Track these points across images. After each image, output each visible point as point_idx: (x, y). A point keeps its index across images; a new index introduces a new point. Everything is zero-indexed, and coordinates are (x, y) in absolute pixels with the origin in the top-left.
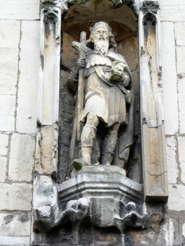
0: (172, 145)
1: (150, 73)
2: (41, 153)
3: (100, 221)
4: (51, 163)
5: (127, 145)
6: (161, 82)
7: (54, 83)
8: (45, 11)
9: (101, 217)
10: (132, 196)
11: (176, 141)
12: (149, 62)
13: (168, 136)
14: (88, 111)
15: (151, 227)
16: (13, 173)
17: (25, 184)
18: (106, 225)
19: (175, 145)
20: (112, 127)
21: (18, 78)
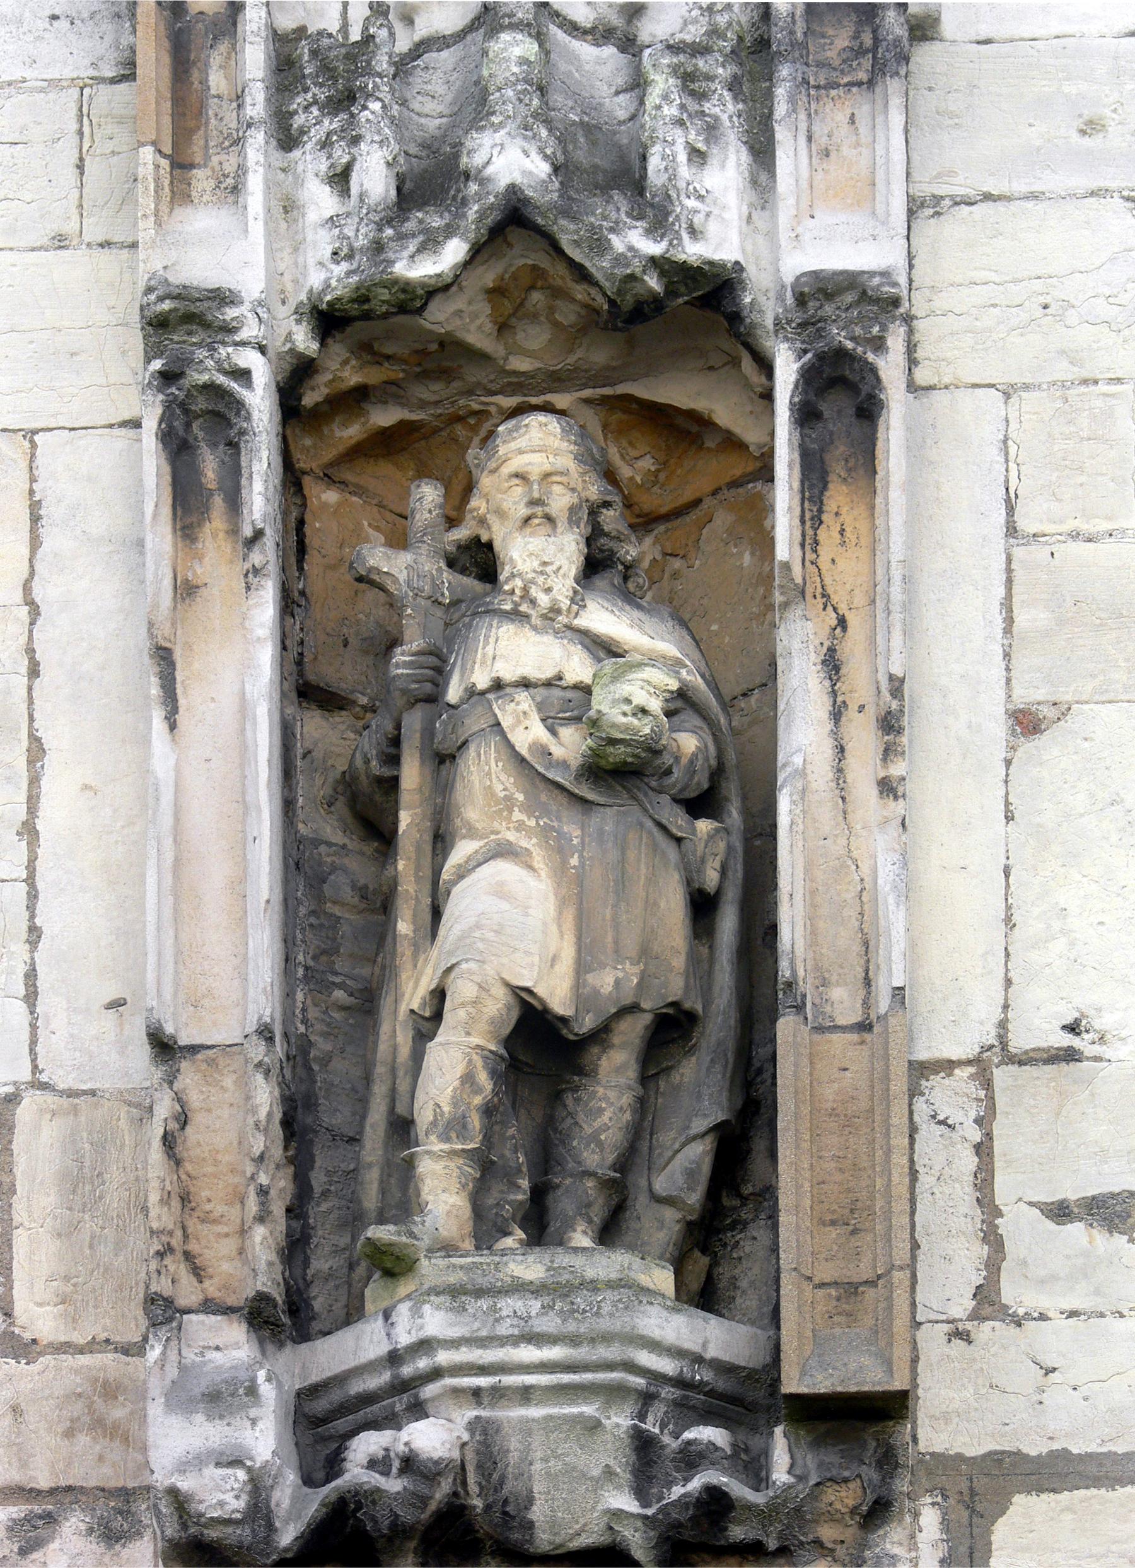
0: (961, 1112)
1: (837, 714)
2: (185, 1198)
3: (531, 1525)
4: (241, 1251)
5: (700, 1125)
6: (897, 769)
7: (245, 806)
8: (168, 377)
9: (535, 1508)
10: (712, 1393)
11: (982, 1094)
12: (832, 650)
13: (922, 1070)
14: (451, 953)
15: (818, 1543)
16: (40, 1305)
17: (110, 1356)
18: (561, 1546)
19: (973, 1114)
20: (600, 1035)
21: (34, 781)
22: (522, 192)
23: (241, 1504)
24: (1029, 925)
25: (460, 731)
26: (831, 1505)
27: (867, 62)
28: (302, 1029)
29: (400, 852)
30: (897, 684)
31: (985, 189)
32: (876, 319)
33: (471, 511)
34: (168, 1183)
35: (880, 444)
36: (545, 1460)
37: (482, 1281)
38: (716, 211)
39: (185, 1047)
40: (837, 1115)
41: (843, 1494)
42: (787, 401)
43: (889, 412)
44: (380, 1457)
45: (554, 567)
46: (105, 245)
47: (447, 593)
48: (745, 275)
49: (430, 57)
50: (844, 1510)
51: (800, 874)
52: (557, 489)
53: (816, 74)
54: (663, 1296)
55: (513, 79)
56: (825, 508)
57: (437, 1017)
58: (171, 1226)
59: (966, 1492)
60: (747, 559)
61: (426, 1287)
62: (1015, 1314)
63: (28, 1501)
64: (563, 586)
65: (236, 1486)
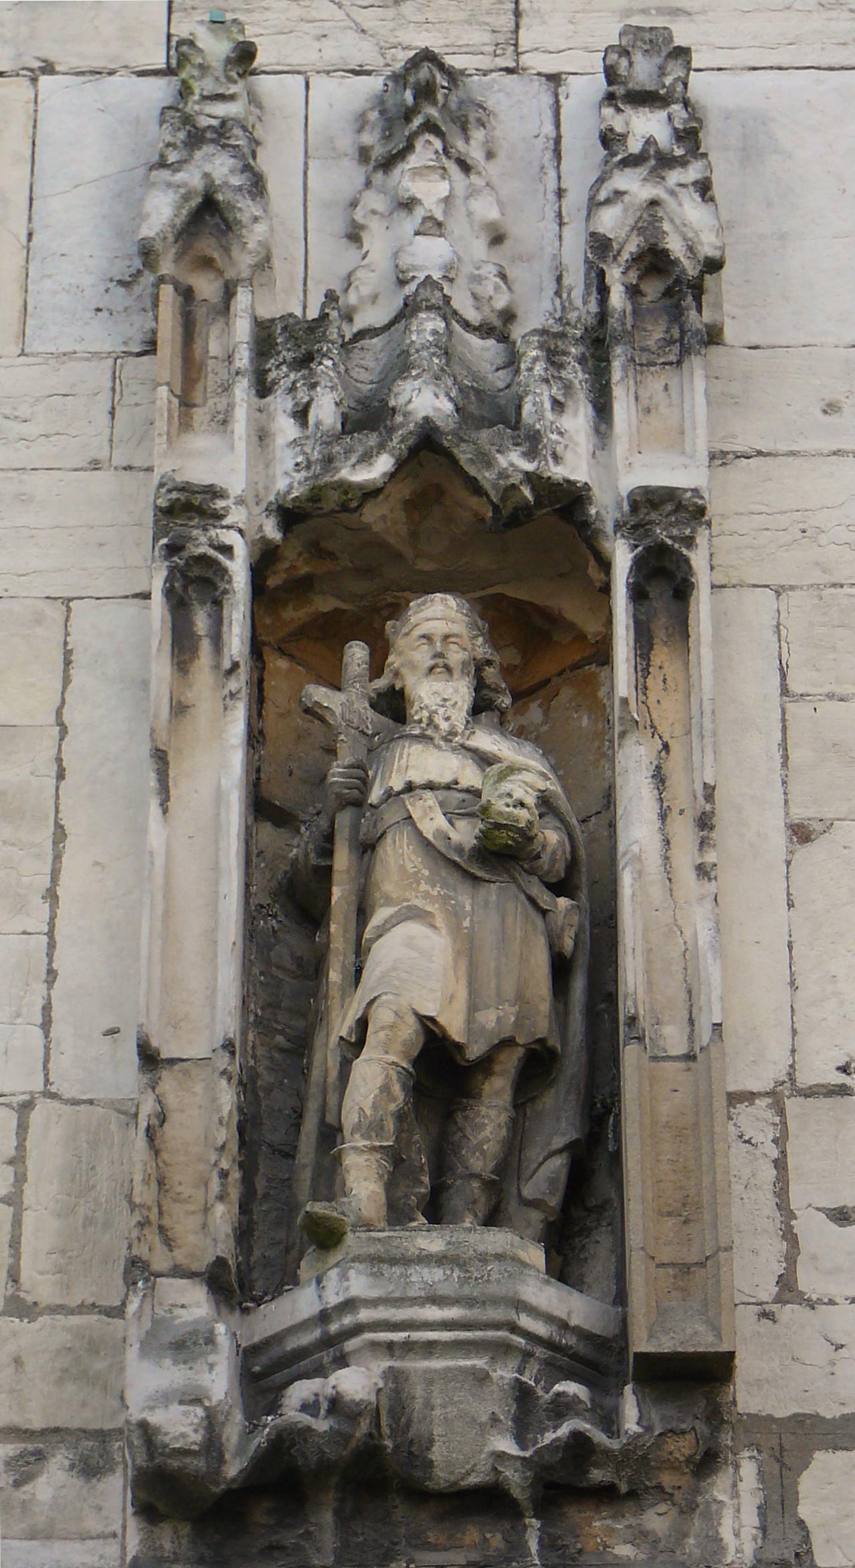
0: (762, 1134)
1: (663, 817)
2: (161, 1183)
3: (430, 1464)
4: (204, 1226)
5: (559, 1142)
6: (711, 857)
9: (434, 1449)
10: (575, 1357)
11: (777, 1120)
12: (658, 768)
13: (735, 1098)
14: (373, 989)
15: (660, 1488)
16: (41, 1273)
17: (95, 1317)
18: (455, 1483)
19: (771, 1136)
20: (485, 1064)
21: (57, 857)
22: (434, 423)
23: (198, 1437)
24: (809, 988)
25: (379, 825)
26: (671, 1453)
27: (676, 349)
28: (252, 1063)
29: (332, 917)
30: (710, 791)
31: (758, 448)
32: (687, 524)
33: (389, 666)
34: (148, 1167)
35: (691, 616)
36: (444, 1406)
37: (396, 1253)
38: (571, 445)
39: (166, 1060)
40: (671, 1127)
41: (681, 1444)
42: (625, 581)
43: (698, 590)
44: (311, 1402)
45: (452, 702)
46: (129, 468)
47: (370, 727)
48: (591, 493)
49: (365, 342)
50: (682, 1459)
51: (639, 935)
52: (453, 647)
53: (640, 356)
54: (539, 1271)
55: (428, 344)
56: (652, 663)
57: (360, 1043)
58: (149, 1203)
59: (777, 1448)
60: (585, 722)
61: (350, 1256)
62: (809, 1300)
63: (24, 1441)
64: (459, 717)
65: (196, 1421)
